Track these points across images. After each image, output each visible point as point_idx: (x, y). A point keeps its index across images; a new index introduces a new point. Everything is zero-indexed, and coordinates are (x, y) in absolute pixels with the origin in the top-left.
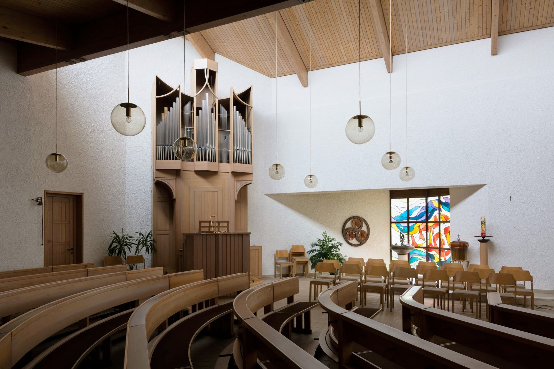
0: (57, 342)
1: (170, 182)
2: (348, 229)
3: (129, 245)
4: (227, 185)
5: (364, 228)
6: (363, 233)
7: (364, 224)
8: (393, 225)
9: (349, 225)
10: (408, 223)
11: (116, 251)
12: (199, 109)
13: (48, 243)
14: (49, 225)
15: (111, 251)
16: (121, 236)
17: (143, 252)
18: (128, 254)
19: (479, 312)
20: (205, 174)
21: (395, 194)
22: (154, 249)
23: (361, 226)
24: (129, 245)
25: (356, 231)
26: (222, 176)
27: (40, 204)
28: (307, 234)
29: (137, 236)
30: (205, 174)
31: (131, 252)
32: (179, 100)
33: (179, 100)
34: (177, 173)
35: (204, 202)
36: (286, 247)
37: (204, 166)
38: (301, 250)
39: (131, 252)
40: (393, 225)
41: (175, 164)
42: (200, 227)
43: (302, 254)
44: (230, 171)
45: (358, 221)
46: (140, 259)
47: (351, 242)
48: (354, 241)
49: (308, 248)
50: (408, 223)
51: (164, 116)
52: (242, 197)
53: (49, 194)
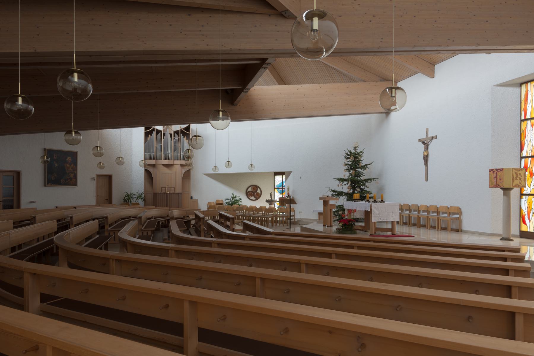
0: (258, 266)
1: (151, 169)
2: (249, 191)
3: (133, 198)
4: (178, 171)
5: (259, 191)
6: (258, 194)
7: (259, 189)
8: (276, 190)
9: (250, 189)
10: (282, 188)
11: (128, 200)
12: (164, 135)
13: (97, 196)
14: (97, 188)
15: (125, 200)
16: (129, 194)
17: (139, 201)
18: (132, 202)
19: (23, 223)
20: (167, 166)
21: (276, 174)
22: (144, 200)
23: (257, 190)
24: (133, 198)
25: (254, 192)
26: (175, 166)
27: (94, 180)
28: (223, 193)
29: (137, 194)
30: (167, 166)
31: (134, 201)
32: (155, 132)
33: (155, 132)
34: (154, 166)
35: (169, 178)
36: (213, 200)
37: (166, 162)
38: (221, 202)
39: (134, 201)
40: (276, 190)
41: (153, 162)
42: (162, 190)
43: (222, 204)
44: (179, 164)
45: (256, 187)
46: (138, 204)
47: (251, 198)
48: (253, 198)
49: (225, 202)
50: (282, 188)
51: (148, 139)
52: (187, 176)
53: (98, 176)
